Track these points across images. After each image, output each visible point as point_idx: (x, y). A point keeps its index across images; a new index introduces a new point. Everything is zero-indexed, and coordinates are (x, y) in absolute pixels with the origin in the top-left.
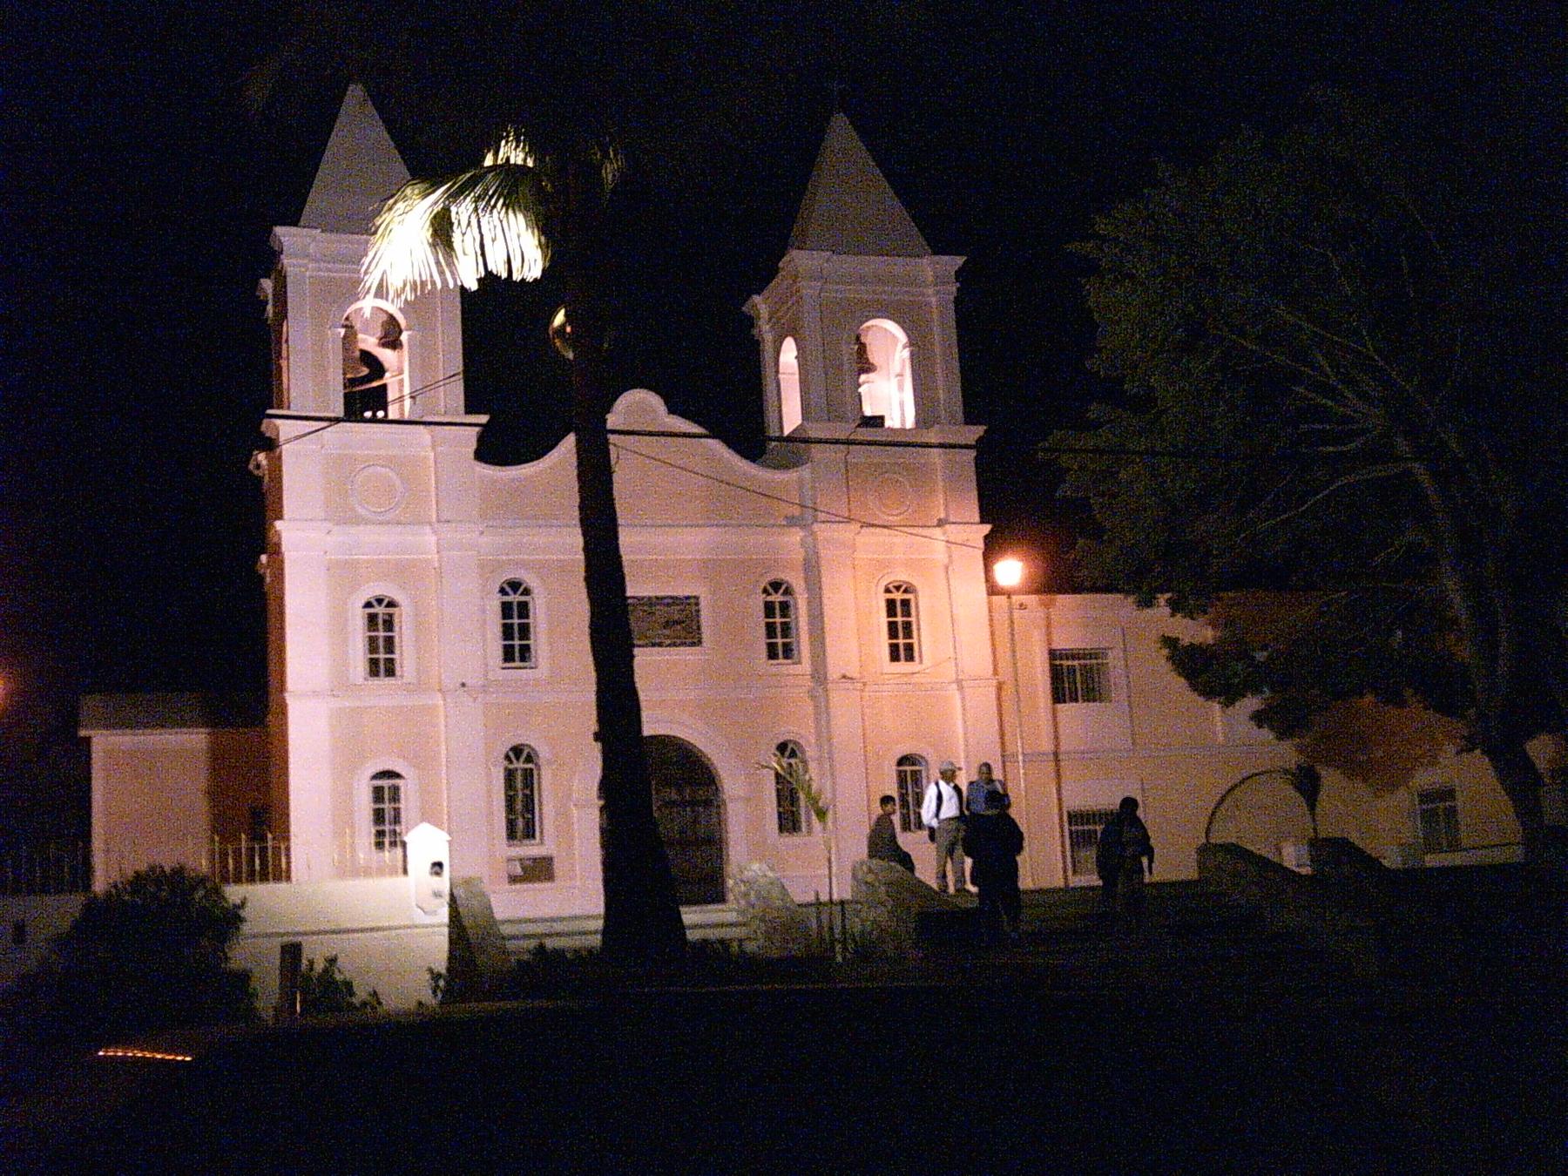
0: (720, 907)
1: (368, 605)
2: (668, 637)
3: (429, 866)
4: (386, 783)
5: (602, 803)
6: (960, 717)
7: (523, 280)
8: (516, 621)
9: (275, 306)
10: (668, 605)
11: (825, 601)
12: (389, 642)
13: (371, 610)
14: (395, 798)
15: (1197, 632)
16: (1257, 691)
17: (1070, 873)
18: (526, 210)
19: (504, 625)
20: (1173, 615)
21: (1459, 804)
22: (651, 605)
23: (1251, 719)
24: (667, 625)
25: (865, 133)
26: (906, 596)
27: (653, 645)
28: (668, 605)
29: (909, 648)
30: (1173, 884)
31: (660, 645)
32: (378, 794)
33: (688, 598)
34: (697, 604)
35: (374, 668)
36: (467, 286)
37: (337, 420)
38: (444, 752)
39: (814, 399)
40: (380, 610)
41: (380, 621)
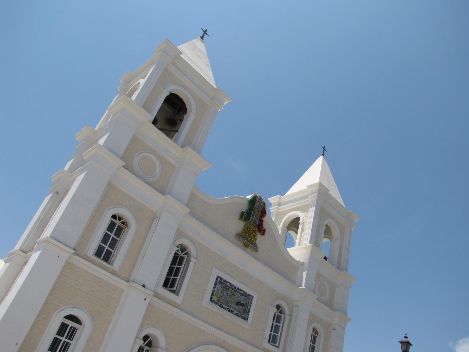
0: (106, 229)
1: (114, 217)
2: (236, 309)
3: (152, 125)
4: (71, 324)
5: (299, 221)
6: (177, 283)
7: (270, 209)
8: (63, 339)
9: (54, 176)
10: (241, 294)
11: (326, 307)
12: (114, 242)
13: (114, 220)
14: (71, 336)
15: (335, 193)
16: (39, 250)
17: (274, 344)
18: (184, 116)
19: (106, 234)
20: (349, 319)
21: (213, 304)
22: (235, 291)
23: (170, 93)
24: (238, 303)
25: (41, 252)
26: (122, 226)
27: (229, 311)
28: (241, 294)
29: (109, 254)
30: (325, 187)
31: (232, 312)
32: (111, 226)
33: (249, 295)
34: (252, 300)
35: (98, 253)
36: (177, 250)
37: (117, 155)
38: (105, 123)
39: (402, 348)
40: (118, 223)
41: (178, 262)
